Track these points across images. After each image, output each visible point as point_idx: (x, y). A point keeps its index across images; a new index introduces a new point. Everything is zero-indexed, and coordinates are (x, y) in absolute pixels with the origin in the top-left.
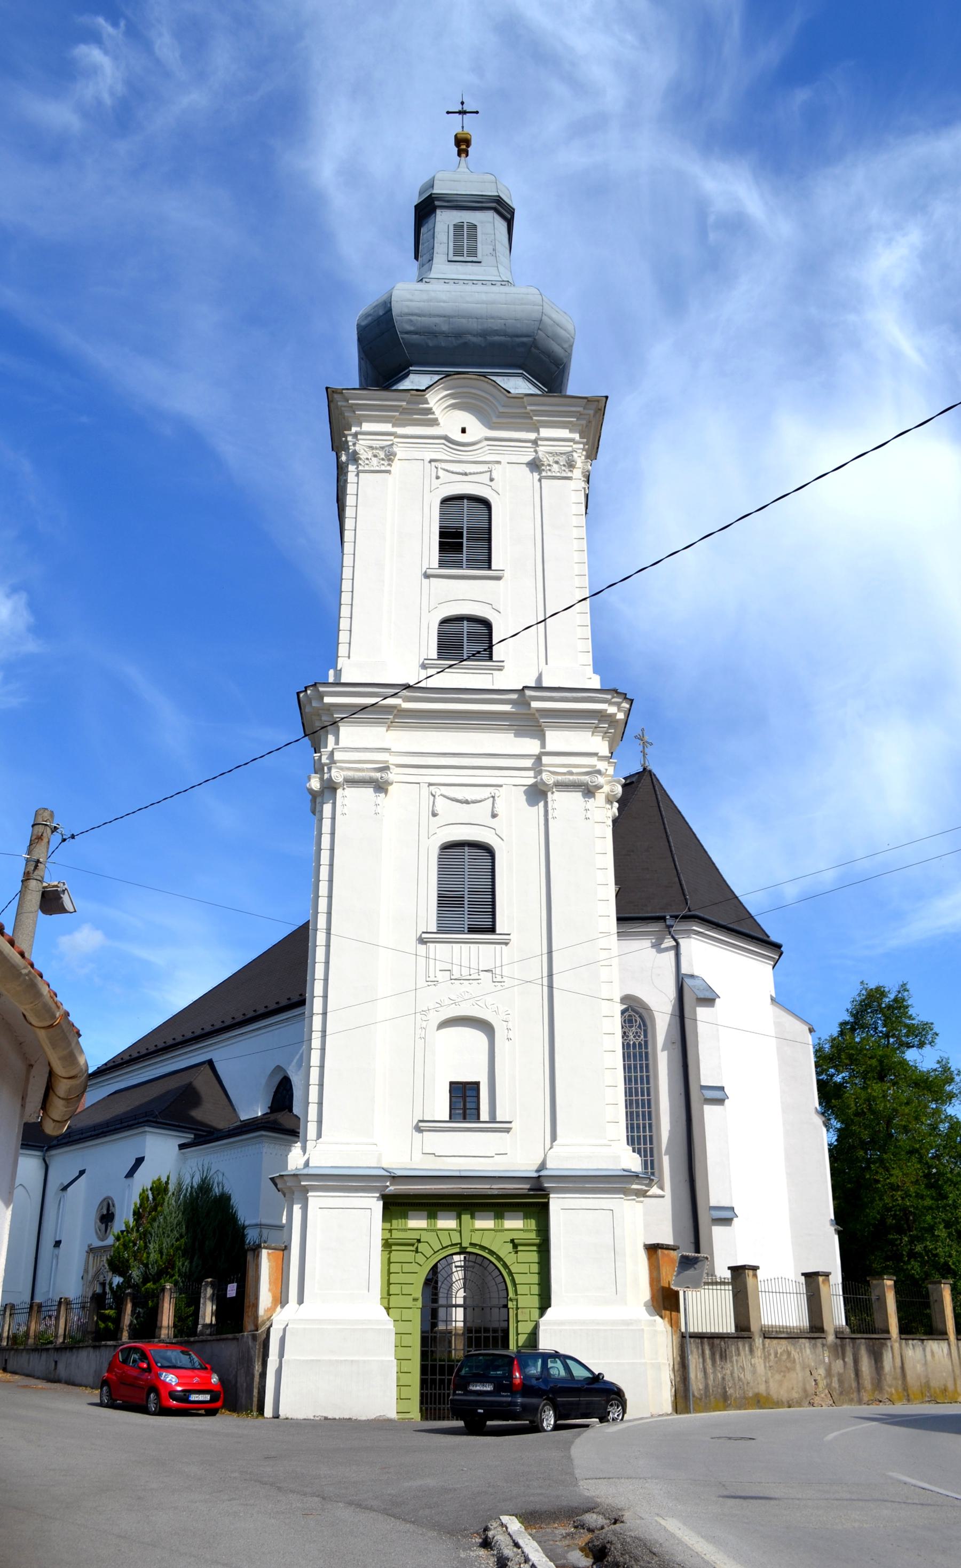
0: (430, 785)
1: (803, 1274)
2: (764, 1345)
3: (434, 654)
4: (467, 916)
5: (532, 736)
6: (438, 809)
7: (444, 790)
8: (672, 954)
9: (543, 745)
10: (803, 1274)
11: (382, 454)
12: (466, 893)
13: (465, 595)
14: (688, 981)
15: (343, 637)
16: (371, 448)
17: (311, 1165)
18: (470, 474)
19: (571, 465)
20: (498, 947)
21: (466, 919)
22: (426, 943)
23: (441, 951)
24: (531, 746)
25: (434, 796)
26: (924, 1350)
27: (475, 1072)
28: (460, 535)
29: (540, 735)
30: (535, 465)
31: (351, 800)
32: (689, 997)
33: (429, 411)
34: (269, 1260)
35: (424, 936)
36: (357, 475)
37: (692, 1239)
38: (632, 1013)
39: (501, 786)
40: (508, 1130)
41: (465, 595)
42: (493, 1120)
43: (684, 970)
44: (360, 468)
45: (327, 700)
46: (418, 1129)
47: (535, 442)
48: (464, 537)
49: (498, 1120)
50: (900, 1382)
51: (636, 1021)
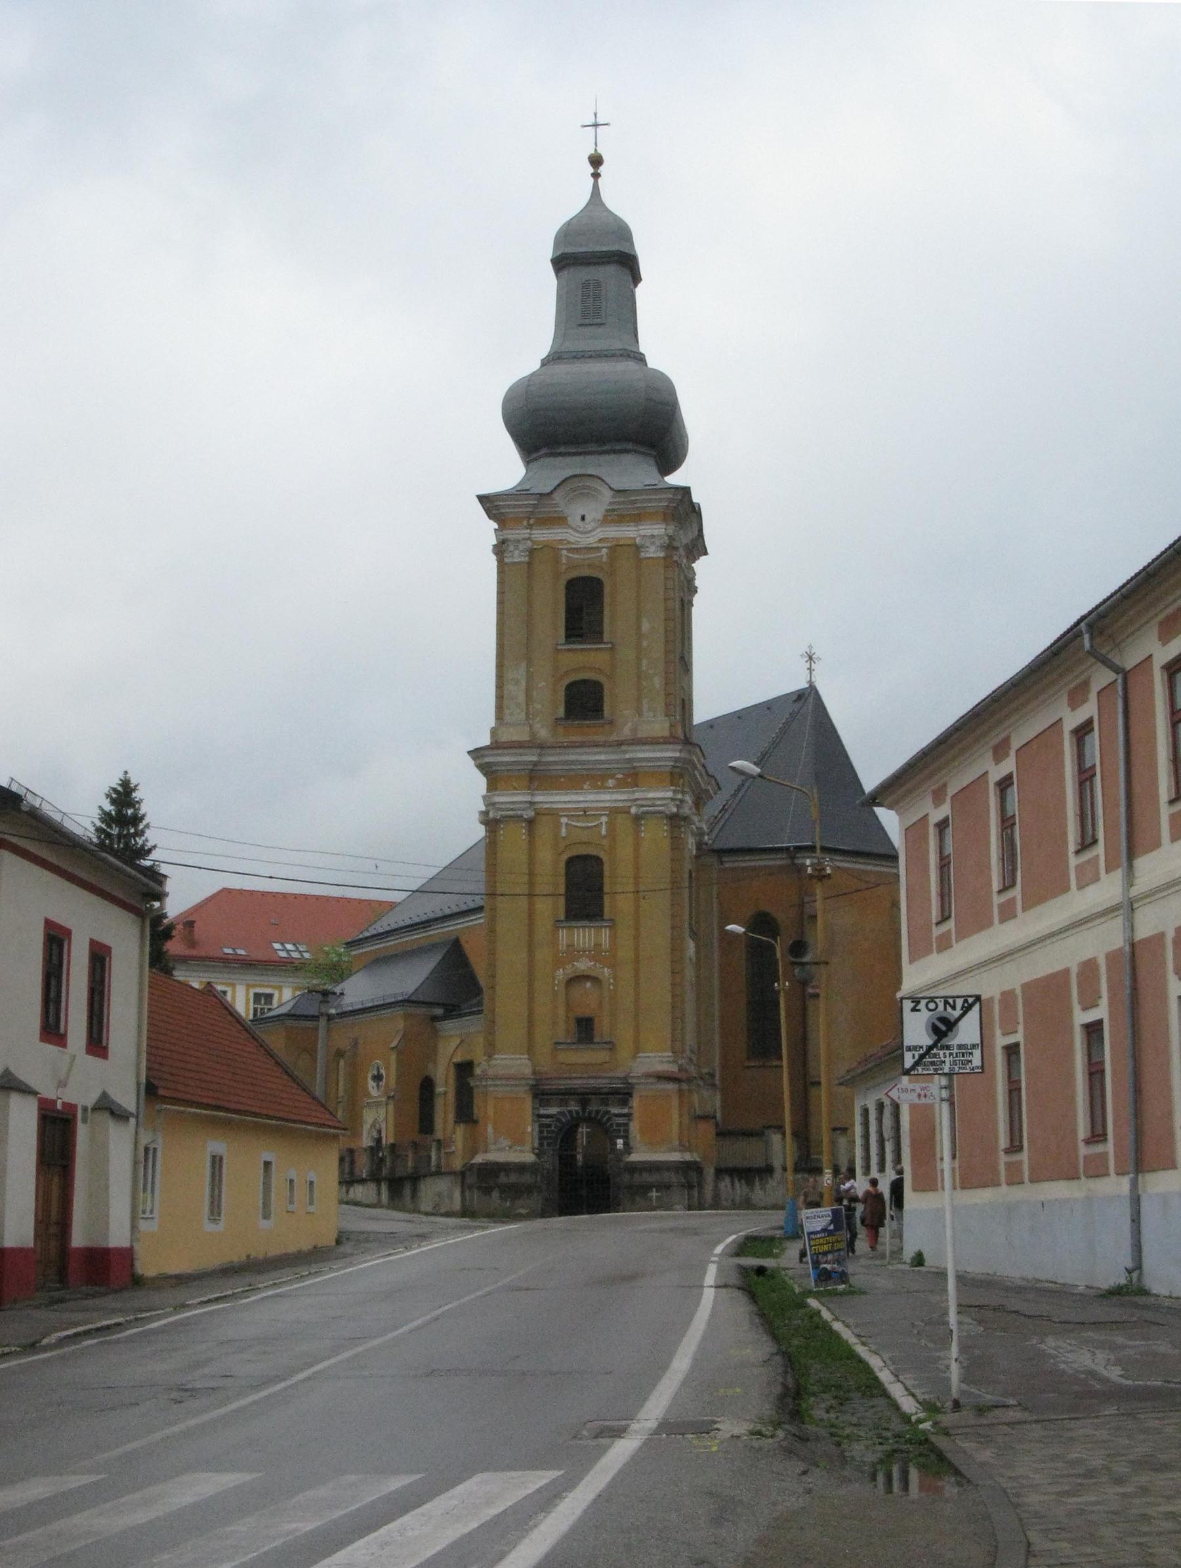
13: (586, 661)
41: (586, 661)
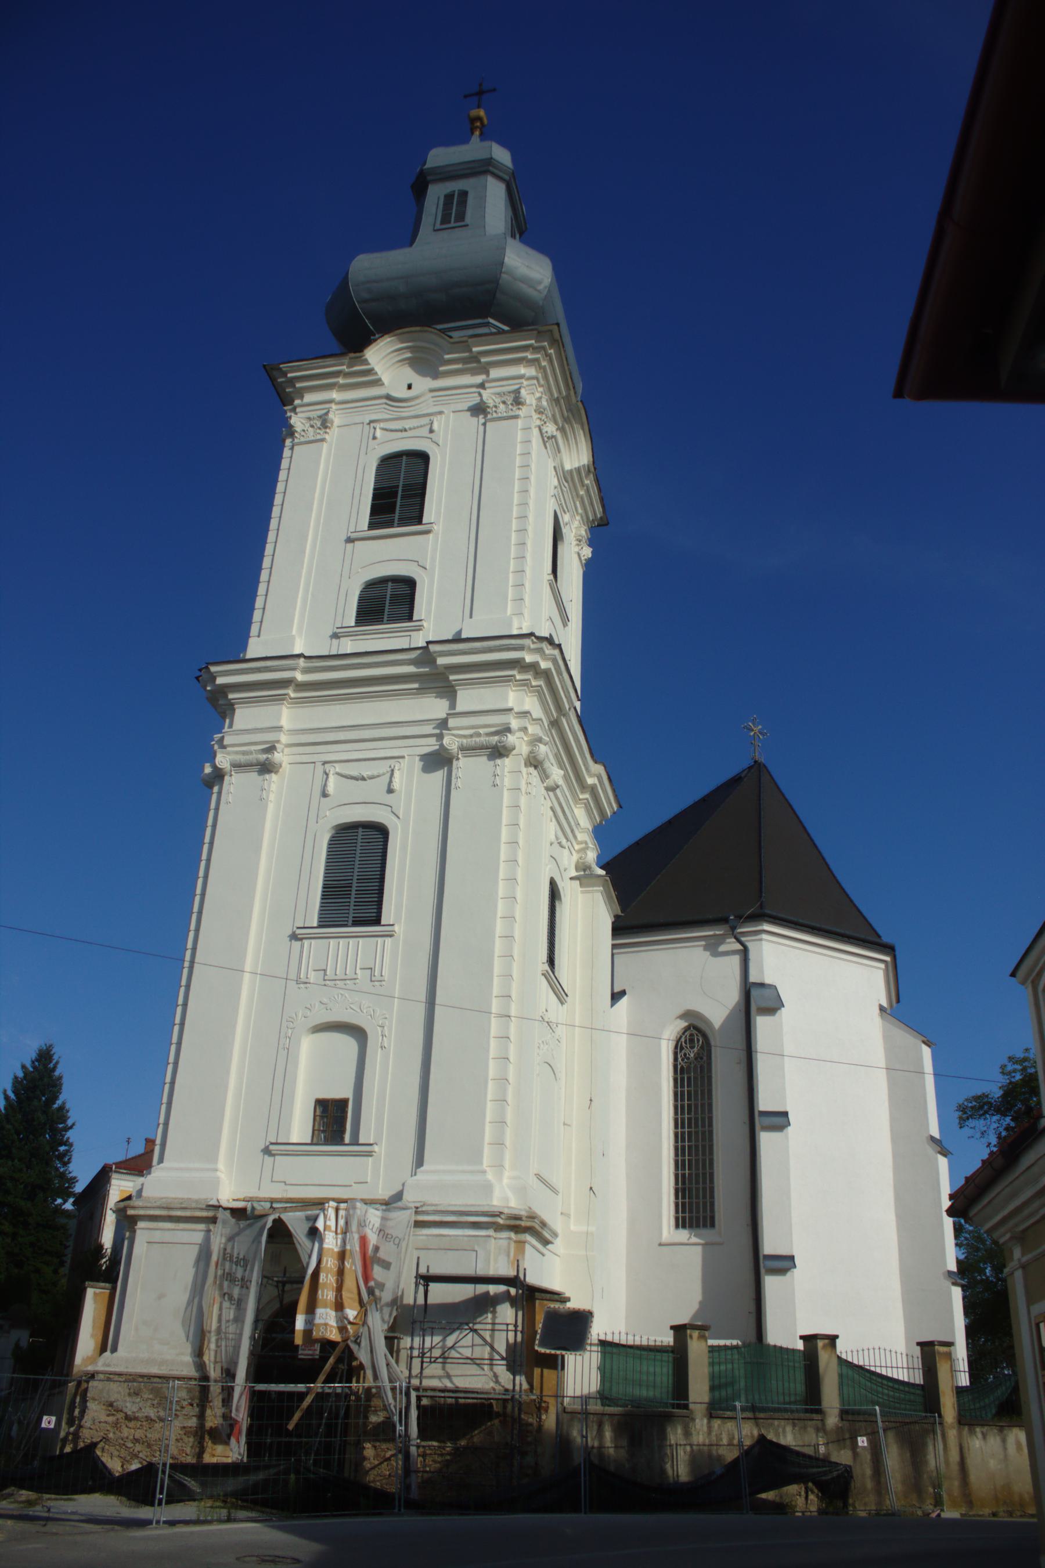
0: (324, 763)
1: (918, 1344)
2: (710, 1428)
3: (351, 619)
4: (352, 907)
5: (440, 695)
6: (331, 788)
7: (338, 768)
8: (736, 960)
9: (453, 705)
10: (918, 1344)
11: (319, 423)
12: (355, 881)
13: (390, 554)
14: (754, 993)
15: (257, 615)
16: (309, 419)
17: (144, 1194)
18: (410, 429)
19: (518, 402)
20: (380, 940)
21: (351, 911)
22: (301, 939)
23: (312, 947)
24: (435, 707)
25: (327, 775)
26: (1004, 1441)
27: (343, 1090)
28: (395, 494)
29: (449, 692)
30: (479, 410)
31: (235, 786)
32: (755, 1000)
33: (370, 372)
34: (95, 1301)
35: (299, 931)
36: (292, 449)
37: (753, 1295)
38: (694, 1032)
39: (403, 757)
40: (369, 1154)
41: (390, 554)
42: (355, 1142)
43: (753, 978)
44: (296, 440)
45: (220, 681)
46: (267, 1151)
47: (482, 386)
48: (399, 494)
49: (361, 1142)
50: (956, 1483)
51: (698, 1040)
